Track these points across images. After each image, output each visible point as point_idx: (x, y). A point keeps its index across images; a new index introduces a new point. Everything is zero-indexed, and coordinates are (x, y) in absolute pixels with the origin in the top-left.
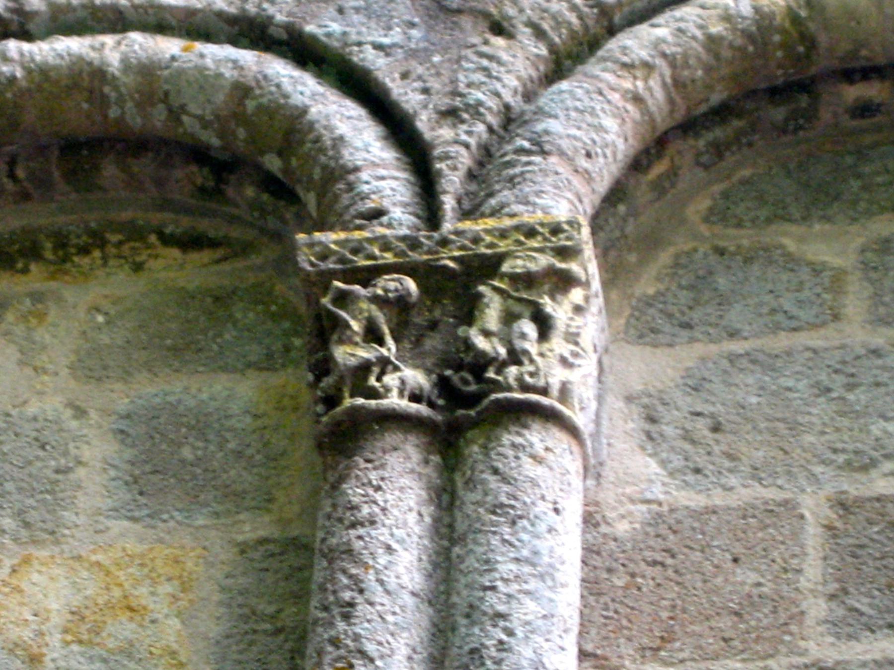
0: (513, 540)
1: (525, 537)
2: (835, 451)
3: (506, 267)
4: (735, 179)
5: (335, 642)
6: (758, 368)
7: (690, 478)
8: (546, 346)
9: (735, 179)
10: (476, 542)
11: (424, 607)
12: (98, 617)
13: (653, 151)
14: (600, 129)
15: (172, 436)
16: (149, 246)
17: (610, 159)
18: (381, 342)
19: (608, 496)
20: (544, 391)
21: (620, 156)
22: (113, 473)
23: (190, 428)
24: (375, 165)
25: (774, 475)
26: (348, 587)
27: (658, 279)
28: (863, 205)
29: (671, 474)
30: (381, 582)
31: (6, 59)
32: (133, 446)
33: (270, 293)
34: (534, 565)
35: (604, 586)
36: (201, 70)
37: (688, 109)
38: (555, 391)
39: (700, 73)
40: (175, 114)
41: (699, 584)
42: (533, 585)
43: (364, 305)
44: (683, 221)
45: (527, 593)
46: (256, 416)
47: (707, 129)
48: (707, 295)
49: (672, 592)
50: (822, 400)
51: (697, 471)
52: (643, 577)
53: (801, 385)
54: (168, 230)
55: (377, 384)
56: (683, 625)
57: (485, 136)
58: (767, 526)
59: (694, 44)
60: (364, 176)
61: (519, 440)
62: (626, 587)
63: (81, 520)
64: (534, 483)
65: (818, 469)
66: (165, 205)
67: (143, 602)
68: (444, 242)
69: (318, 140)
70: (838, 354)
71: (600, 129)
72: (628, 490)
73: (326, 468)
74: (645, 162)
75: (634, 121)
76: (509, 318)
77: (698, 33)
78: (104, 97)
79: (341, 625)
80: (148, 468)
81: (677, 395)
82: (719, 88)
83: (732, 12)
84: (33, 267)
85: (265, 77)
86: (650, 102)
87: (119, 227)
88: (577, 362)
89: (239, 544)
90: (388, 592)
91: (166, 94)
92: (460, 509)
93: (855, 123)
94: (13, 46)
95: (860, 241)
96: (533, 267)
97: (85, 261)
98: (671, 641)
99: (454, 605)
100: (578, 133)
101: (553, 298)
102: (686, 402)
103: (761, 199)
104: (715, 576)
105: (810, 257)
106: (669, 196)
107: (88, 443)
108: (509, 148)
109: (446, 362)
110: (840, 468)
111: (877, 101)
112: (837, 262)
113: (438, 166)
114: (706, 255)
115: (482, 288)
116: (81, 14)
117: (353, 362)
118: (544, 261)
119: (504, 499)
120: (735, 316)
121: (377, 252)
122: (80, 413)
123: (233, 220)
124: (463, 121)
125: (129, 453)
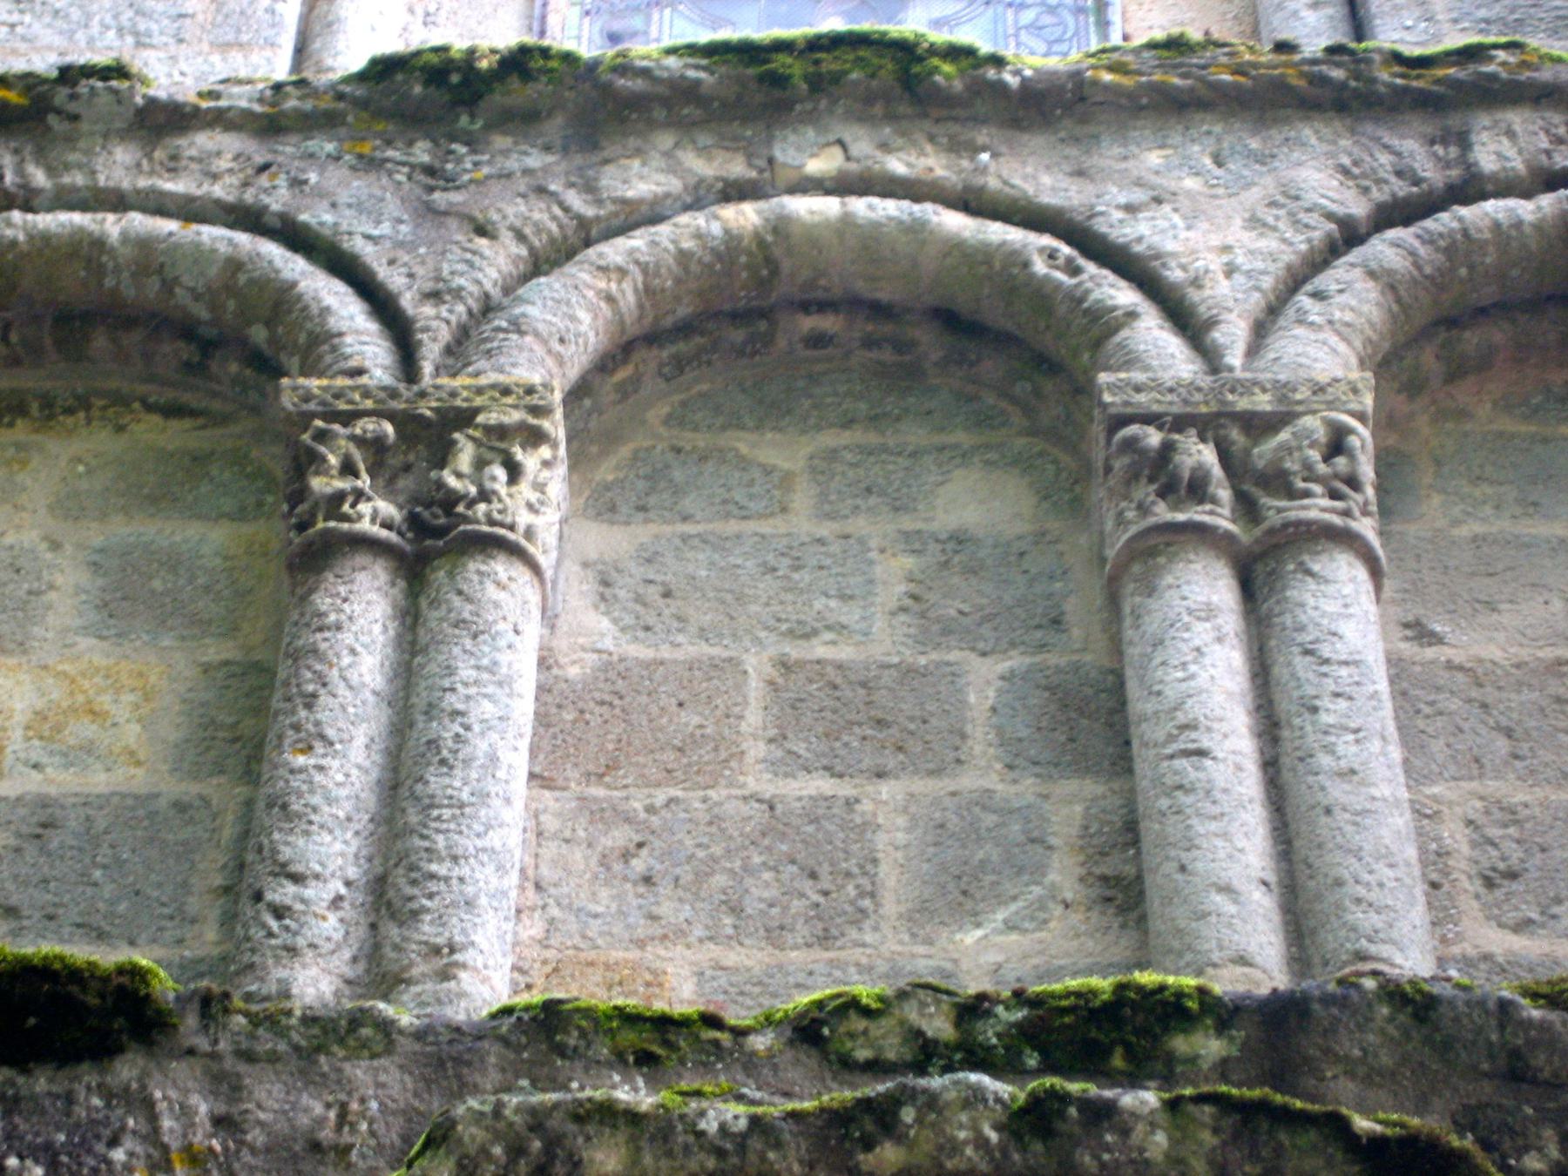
0: (474, 649)
1: (486, 649)
2: (779, 620)
3: (480, 419)
4: (695, 391)
5: (297, 727)
6: (708, 548)
7: (641, 634)
8: (514, 489)
9: (695, 391)
10: (439, 652)
11: (384, 705)
12: (61, 718)
13: (619, 357)
14: (573, 318)
15: (144, 569)
16: (132, 412)
17: (582, 349)
18: (356, 475)
19: (561, 643)
20: (512, 528)
21: (590, 349)
22: (84, 597)
23: (162, 564)
24: (357, 332)
25: (721, 636)
26: (311, 681)
27: (617, 468)
28: (812, 421)
29: (623, 630)
30: (345, 679)
31: (9, 224)
32: (105, 575)
33: (246, 456)
34: (494, 674)
35: (554, 720)
36: (197, 246)
37: (656, 318)
38: (521, 528)
39: (669, 283)
40: (169, 286)
41: (644, 723)
42: (490, 689)
43: (343, 442)
44: (643, 422)
45: (485, 696)
46: (226, 558)
47: (672, 342)
48: (663, 484)
49: (618, 729)
50: (768, 577)
51: (647, 628)
52: (592, 713)
53: (749, 564)
54: (152, 400)
55: (352, 511)
56: (627, 756)
57: (464, 317)
58: (710, 679)
59: (666, 256)
60: (348, 339)
61: (483, 568)
62: (574, 722)
63: (50, 635)
64: (497, 605)
65: (763, 634)
66: (151, 379)
67: (106, 707)
68: (423, 394)
69: (305, 308)
70: (785, 541)
71: (573, 318)
72: (581, 640)
73: (294, 585)
74: (611, 365)
75: (605, 318)
76: (480, 464)
77: (671, 247)
78: (101, 266)
79: (303, 713)
80: (119, 595)
81: (632, 566)
82: (685, 301)
83: (703, 231)
84: (19, 422)
85: (258, 254)
86: (622, 303)
87: (100, 394)
88: (543, 509)
89: (203, 664)
90: (351, 688)
91: (162, 266)
92: (424, 624)
93: (808, 353)
94: (16, 215)
95: (810, 449)
96: (506, 420)
97: (70, 421)
98: (617, 768)
99: (412, 706)
100: (554, 320)
101: (523, 448)
102: (639, 571)
103: (717, 410)
104: (661, 716)
105: (762, 459)
106: (631, 401)
107: (62, 571)
108: (488, 327)
109: (415, 500)
110: (782, 634)
111: (831, 332)
112: (786, 465)
113: (419, 336)
114: (663, 452)
115: (456, 435)
116: (88, 194)
117: (329, 490)
118: (516, 416)
119: (466, 615)
120: (688, 503)
121: (357, 397)
122: (56, 546)
123: (215, 395)
124: (444, 302)
125: (100, 582)
